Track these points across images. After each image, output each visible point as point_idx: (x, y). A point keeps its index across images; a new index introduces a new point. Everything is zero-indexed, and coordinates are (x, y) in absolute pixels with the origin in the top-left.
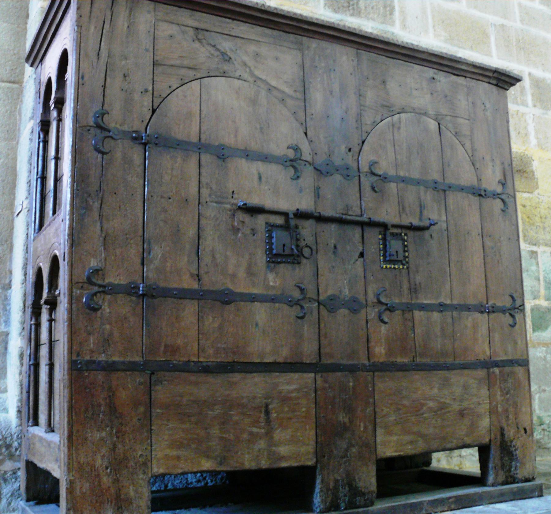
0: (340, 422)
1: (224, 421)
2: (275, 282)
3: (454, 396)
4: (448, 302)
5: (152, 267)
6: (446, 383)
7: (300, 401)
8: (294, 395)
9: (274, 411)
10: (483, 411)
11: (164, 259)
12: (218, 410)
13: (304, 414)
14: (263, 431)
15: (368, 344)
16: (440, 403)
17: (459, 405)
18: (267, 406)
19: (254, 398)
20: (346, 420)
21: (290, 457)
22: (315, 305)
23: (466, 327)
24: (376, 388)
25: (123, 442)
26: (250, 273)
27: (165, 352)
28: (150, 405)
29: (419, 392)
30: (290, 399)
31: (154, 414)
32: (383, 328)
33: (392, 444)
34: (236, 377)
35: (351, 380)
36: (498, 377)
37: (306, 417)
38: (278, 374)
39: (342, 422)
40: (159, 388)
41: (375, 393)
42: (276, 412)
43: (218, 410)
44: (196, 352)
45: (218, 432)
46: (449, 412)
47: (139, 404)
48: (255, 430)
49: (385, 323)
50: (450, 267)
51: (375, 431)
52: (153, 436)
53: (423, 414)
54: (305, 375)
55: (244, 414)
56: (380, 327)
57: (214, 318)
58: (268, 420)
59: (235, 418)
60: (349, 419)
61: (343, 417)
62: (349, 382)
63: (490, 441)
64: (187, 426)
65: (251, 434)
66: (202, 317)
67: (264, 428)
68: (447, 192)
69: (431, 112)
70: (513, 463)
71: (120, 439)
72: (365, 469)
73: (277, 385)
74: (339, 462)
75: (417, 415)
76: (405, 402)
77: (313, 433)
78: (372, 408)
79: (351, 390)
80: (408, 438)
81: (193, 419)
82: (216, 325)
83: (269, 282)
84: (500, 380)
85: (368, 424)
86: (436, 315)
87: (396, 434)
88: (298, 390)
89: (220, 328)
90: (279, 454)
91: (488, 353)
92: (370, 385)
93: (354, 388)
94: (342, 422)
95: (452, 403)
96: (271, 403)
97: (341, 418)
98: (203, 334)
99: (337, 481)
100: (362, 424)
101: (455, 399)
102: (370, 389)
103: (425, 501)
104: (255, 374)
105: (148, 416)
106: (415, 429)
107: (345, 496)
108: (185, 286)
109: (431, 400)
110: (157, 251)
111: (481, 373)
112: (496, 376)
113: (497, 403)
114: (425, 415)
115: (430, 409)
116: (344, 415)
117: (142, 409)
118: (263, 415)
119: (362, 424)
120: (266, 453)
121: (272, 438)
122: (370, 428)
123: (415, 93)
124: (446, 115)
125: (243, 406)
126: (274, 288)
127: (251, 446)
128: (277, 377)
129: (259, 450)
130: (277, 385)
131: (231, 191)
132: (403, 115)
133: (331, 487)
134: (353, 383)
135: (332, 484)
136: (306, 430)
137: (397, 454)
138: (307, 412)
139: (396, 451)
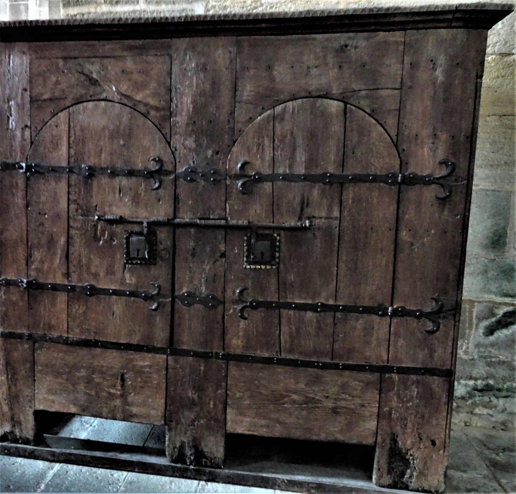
0: (189, 397)
1: (89, 381)
2: (131, 280)
3: (327, 393)
4: (331, 302)
5: (33, 267)
6: (316, 380)
7: (152, 375)
8: (148, 369)
9: (128, 380)
10: (368, 414)
11: (42, 262)
12: (83, 373)
13: (155, 386)
14: (119, 393)
15: (223, 336)
16: (307, 397)
17: (333, 403)
18: (122, 375)
19: (112, 367)
20: (196, 396)
21: (140, 416)
22: (168, 300)
23: (355, 328)
24: (230, 375)
25: (15, 385)
26: (110, 272)
27: (44, 329)
28: (34, 363)
29: (282, 385)
30: (144, 372)
31: (36, 370)
32: (242, 324)
33: (244, 424)
34: (98, 351)
35: (202, 365)
36: (396, 383)
37: (156, 388)
38: (133, 352)
39: (191, 398)
40: (39, 352)
41: (228, 379)
42: (130, 380)
43: (83, 373)
44: (66, 330)
45: (83, 388)
46: (318, 407)
47: (27, 361)
48: (112, 391)
49: (245, 319)
50: (337, 267)
51: (226, 410)
52: (36, 384)
53: (283, 404)
54: (158, 356)
55: (104, 379)
56: (240, 322)
57: (79, 306)
58: (123, 386)
59: (97, 380)
60: (198, 396)
61: (192, 394)
62: (200, 366)
63: (375, 443)
64: (60, 380)
65: (109, 393)
66: (71, 305)
67: (119, 391)
68: (346, 185)
69: (335, 91)
70: (409, 471)
71: (13, 383)
72: (212, 439)
73: (132, 360)
74: (186, 428)
75: (275, 404)
76: (263, 391)
77: (163, 401)
78: (224, 391)
79: (202, 373)
80: (263, 422)
81: (64, 376)
82: (81, 311)
83: (125, 280)
84: (398, 386)
85: (217, 403)
86: (309, 314)
87: (249, 417)
88: (150, 366)
89: (85, 313)
90: (131, 412)
91: (385, 357)
92: (223, 371)
93: (205, 371)
94: (191, 398)
95: (323, 400)
96: (126, 373)
97: (190, 394)
98: (70, 317)
99: (183, 443)
100: (212, 403)
101: (327, 397)
102: (223, 374)
103: (279, 479)
104: (114, 351)
105: (32, 370)
106: (273, 416)
107: (191, 455)
108: (59, 282)
109: (294, 393)
110: (37, 255)
111: (374, 377)
112: (393, 382)
113: (391, 409)
114: (286, 405)
115: (294, 402)
116: (193, 392)
117: (28, 365)
118: (119, 381)
119: (212, 403)
120: (120, 410)
121: (126, 399)
122: (220, 407)
123: (314, 72)
124: (360, 90)
125: (103, 373)
126: (130, 284)
127: (109, 402)
128: (132, 354)
129: (115, 406)
130: (132, 360)
131: (95, 204)
132: (290, 104)
133: (178, 446)
134: (204, 368)
135: (178, 444)
136: (156, 398)
137: (250, 433)
138: (158, 384)
139: (248, 431)
